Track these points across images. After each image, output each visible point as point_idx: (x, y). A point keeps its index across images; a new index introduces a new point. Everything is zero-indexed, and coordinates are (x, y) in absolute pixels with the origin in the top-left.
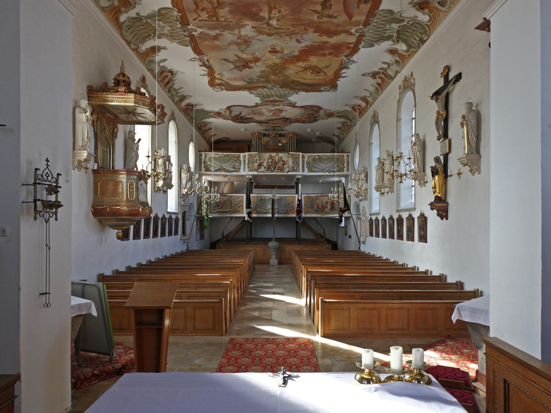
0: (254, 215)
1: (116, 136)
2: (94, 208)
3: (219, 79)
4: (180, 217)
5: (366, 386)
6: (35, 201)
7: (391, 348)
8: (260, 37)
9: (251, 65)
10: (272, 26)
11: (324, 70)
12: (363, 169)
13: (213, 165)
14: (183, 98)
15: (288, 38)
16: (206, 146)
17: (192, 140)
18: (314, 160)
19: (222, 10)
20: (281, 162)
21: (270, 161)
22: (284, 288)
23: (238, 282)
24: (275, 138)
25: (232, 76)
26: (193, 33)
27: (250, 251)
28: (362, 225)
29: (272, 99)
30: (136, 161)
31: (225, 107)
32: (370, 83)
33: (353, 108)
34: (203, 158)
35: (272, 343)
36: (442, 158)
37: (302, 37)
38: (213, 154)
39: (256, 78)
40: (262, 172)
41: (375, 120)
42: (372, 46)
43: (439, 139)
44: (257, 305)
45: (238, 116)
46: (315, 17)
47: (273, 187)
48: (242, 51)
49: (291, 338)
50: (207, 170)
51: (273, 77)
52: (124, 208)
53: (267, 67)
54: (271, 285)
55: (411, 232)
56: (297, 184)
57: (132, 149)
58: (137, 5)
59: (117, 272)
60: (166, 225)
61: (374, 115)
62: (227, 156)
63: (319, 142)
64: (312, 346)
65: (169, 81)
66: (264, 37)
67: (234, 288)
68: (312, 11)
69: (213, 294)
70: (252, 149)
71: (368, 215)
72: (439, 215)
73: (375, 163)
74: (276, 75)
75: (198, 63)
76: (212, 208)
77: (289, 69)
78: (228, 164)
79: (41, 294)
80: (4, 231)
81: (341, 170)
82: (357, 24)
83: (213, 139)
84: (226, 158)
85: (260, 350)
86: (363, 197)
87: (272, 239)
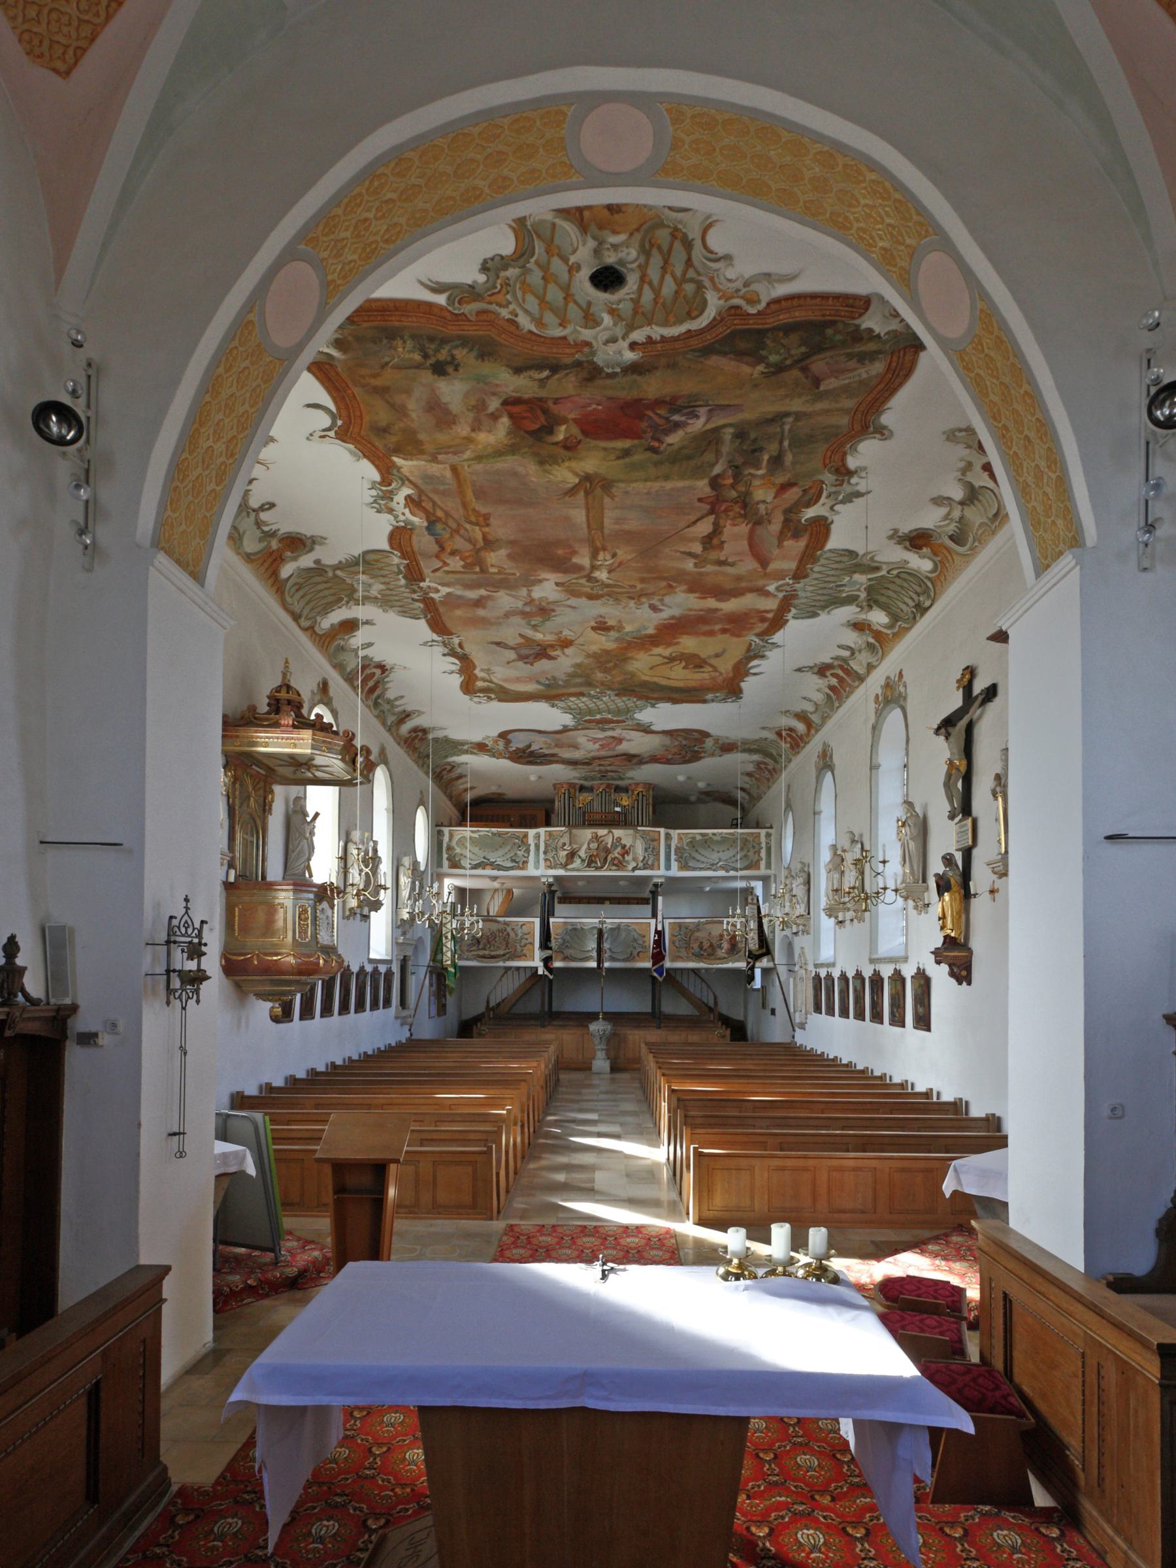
0: (557, 964)
1: (270, 809)
2: (227, 960)
3: (484, 680)
4: (396, 969)
5: (733, 1283)
6: (168, 972)
7: (773, 1226)
8: (573, 601)
9: (553, 654)
10: (597, 581)
11: (713, 661)
12: (799, 866)
13: (469, 854)
14: (406, 716)
15: (632, 603)
16: (453, 812)
17: (422, 802)
18: (693, 843)
19: (492, 554)
20: (619, 849)
21: (594, 845)
22: (622, 1125)
23: (522, 1111)
24: (605, 796)
25: (511, 673)
26: (432, 595)
27: (549, 1042)
28: (799, 988)
29: (598, 717)
30: (309, 859)
31: (496, 734)
32: (814, 688)
33: (779, 734)
34: (446, 839)
35: (593, 1236)
36: (959, 857)
37: (661, 600)
38: (467, 832)
39: (563, 677)
40: (577, 869)
41: (826, 763)
42: (814, 615)
43: (952, 817)
44: (563, 1159)
45: (523, 751)
46: (690, 565)
47: (600, 900)
48: (535, 627)
49: (632, 1225)
50: (455, 865)
51: (599, 676)
52: (287, 959)
53: (588, 656)
54: (593, 1116)
55: (899, 1007)
56: (654, 894)
57: (302, 835)
58: (317, 547)
59: (269, 1088)
60: (365, 989)
61: (824, 751)
62: (499, 835)
63: (704, 802)
64: (673, 1241)
65: (378, 682)
66: (583, 601)
67: (515, 1124)
68: (682, 553)
69: (472, 1136)
70: (554, 817)
71: (811, 967)
72: (952, 974)
73: (825, 856)
74: (606, 671)
75: (440, 649)
76: (465, 948)
77: (636, 660)
78: (501, 852)
79: (170, 1135)
80: (114, 1025)
81: (754, 865)
82: (780, 575)
83: (469, 797)
84: (497, 838)
85: (569, 1248)
86: (801, 927)
87: (598, 1014)
